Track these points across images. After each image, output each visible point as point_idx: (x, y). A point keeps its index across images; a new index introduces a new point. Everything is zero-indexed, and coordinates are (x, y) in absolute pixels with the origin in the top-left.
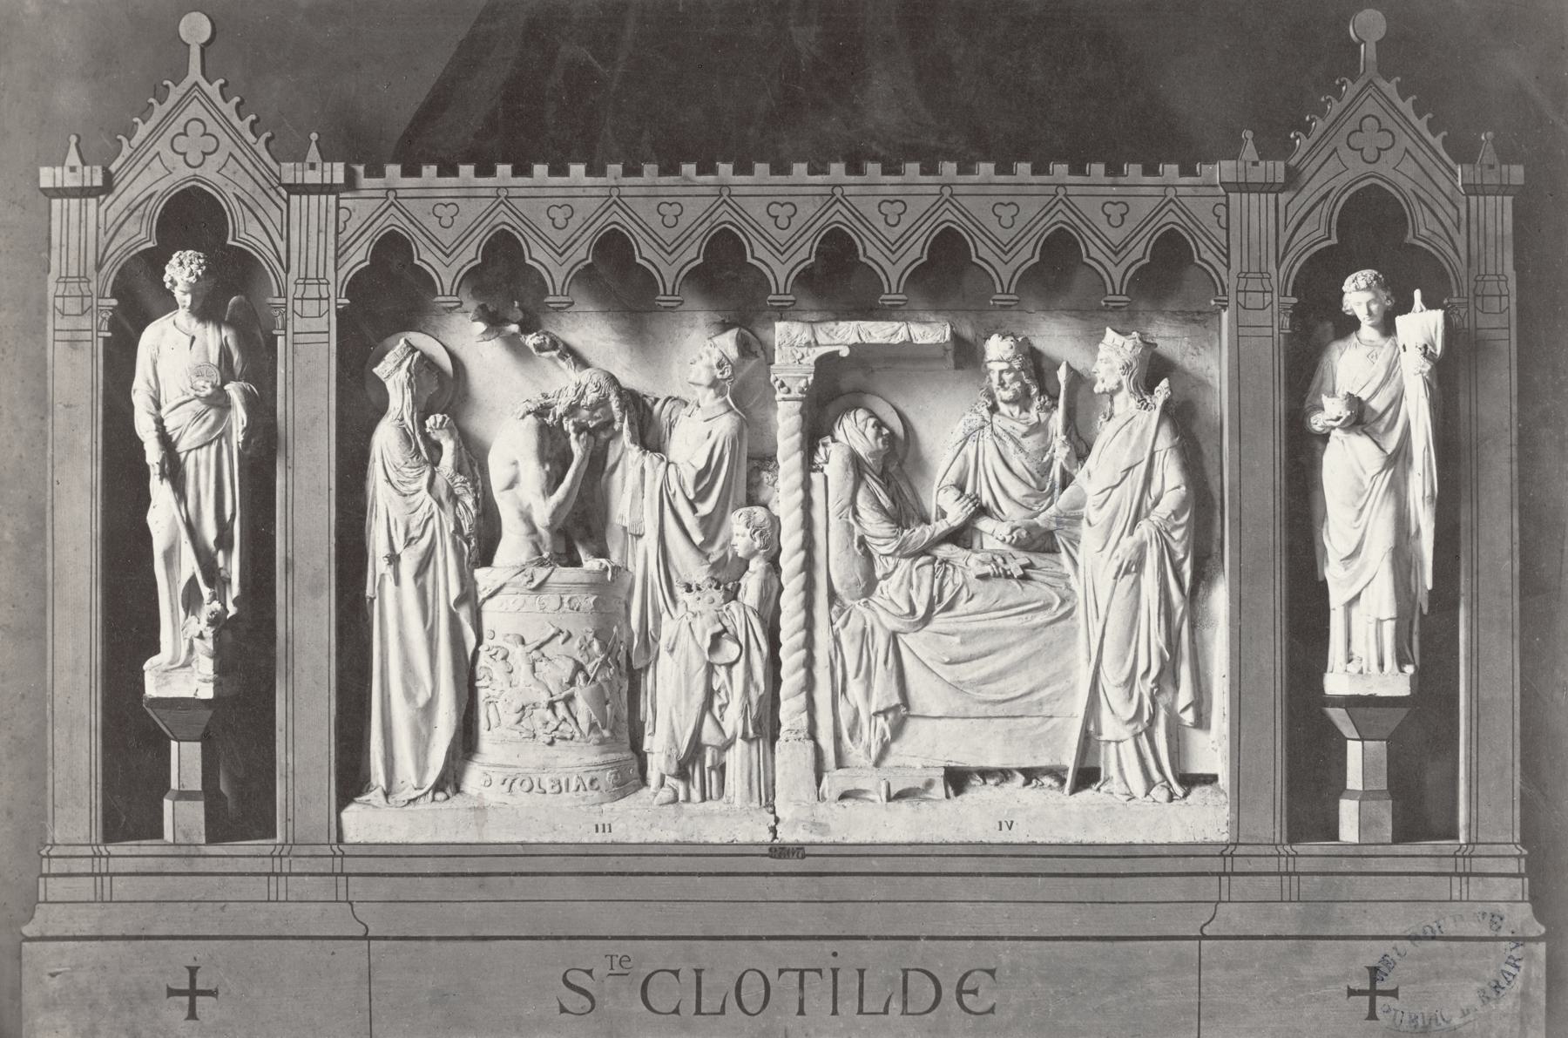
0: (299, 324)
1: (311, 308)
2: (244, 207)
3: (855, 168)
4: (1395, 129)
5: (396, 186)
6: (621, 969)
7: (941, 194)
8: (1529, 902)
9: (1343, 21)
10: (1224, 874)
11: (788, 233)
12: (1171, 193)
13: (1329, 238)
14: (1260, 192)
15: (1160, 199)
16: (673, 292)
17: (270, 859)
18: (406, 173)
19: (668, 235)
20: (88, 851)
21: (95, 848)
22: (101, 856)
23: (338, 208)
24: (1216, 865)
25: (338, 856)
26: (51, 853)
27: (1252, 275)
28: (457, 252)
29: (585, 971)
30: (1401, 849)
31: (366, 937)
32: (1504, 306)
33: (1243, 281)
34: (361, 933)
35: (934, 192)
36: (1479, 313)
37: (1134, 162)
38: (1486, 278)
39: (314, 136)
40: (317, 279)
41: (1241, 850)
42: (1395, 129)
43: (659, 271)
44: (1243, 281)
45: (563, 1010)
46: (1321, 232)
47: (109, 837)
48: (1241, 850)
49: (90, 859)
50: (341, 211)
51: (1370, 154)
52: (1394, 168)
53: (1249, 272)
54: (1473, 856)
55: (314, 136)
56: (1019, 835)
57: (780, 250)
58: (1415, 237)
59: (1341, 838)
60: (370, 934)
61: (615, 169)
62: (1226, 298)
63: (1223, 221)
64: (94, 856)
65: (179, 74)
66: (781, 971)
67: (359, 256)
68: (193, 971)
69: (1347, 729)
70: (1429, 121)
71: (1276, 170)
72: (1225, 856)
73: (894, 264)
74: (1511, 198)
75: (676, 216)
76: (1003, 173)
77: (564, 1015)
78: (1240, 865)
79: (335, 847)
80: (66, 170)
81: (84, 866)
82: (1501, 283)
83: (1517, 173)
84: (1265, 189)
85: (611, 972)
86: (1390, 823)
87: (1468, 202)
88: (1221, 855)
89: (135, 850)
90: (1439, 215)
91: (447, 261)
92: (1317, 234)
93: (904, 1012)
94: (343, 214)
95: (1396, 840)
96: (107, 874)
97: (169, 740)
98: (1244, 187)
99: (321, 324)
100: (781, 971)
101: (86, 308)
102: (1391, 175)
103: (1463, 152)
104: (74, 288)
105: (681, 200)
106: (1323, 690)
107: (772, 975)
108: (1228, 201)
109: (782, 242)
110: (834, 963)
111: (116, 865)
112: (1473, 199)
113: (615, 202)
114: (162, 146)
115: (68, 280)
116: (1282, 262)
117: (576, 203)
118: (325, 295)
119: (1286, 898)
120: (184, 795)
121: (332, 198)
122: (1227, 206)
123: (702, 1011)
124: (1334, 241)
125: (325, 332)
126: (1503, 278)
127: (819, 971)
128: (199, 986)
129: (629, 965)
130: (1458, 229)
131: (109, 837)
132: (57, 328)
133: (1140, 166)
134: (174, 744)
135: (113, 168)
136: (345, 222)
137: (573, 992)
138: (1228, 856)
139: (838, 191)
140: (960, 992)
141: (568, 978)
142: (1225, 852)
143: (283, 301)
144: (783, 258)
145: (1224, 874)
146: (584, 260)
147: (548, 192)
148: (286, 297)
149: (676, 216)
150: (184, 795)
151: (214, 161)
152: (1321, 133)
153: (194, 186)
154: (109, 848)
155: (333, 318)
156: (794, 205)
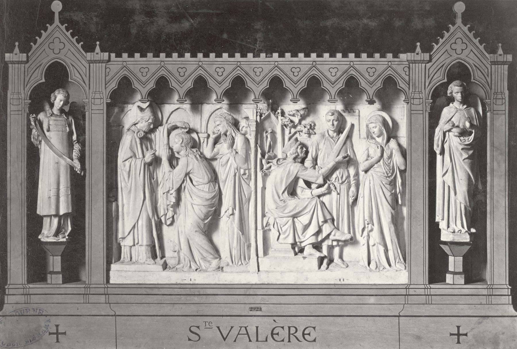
0: (94, 107)
4: (467, 43)
5: (126, 60)
7: (313, 64)
8: (512, 304)
11: (184, 78)
12: (125, 63)
14: (501, 65)
17: (84, 289)
19: (333, 79)
20: (423, 286)
21: (425, 285)
22: (428, 288)
23: (106, 69)
24: (403, 292)
26: (493, 288)
28: (147, 83)
29: (196, 327)
31: (115, 315)
33: (94, 94)
34: (114, 314)
36: (494, 105)
37: (88, 52)
38: (498, 93)
39: (17, 44)
41: (411, 286)
42: (467, 43)
43: (110, 91)
46: (39, 77)
48: (411, 286)
49: (104, 289)
51: (57, 51)
53: (415, 92)
54: (9, 289)
55: (17, 44)
56: (346, 282)
60: (116, 314)
63: (407, 74)
64: (425, 288)
65: (51, 22)
67: (113, 85)
68: (458, 327)
70: (76, 39)
71: (427, 56)
72: (488, 289)
73: (333, 88)
74: (507, 66)
76: (307, 57)
78: (412, 292)
80: (415, 54)
81: (422, 292)
82: (503, 95)
83: (510, 58)
84: (421, 62)
85: (206, 327)
98: (415, 62)
102: (63, 57)
103: (493, 51)
104: (15, 96)
105: (263, 66)
108: (409, 66)
109: (220, 81)
111: (433, 292)
112: (91, 65)
114: (448, 47)
118: (21, 98)
119: (26, 302)
122: (409, 68)
129: (212, 325)
130: (488, 76)
132: (412, 109)
133: (165, 54)
135: (29, 54)
136: (108, 72)
137: (193, 334)
138: (408, 288)
139: (352, 63)
142: (407, 287)
143: (88, 100)
144: (182, 86)
147: (330, 63)
151: (466, 52)
153: (56, 61)
154: (430, 285)
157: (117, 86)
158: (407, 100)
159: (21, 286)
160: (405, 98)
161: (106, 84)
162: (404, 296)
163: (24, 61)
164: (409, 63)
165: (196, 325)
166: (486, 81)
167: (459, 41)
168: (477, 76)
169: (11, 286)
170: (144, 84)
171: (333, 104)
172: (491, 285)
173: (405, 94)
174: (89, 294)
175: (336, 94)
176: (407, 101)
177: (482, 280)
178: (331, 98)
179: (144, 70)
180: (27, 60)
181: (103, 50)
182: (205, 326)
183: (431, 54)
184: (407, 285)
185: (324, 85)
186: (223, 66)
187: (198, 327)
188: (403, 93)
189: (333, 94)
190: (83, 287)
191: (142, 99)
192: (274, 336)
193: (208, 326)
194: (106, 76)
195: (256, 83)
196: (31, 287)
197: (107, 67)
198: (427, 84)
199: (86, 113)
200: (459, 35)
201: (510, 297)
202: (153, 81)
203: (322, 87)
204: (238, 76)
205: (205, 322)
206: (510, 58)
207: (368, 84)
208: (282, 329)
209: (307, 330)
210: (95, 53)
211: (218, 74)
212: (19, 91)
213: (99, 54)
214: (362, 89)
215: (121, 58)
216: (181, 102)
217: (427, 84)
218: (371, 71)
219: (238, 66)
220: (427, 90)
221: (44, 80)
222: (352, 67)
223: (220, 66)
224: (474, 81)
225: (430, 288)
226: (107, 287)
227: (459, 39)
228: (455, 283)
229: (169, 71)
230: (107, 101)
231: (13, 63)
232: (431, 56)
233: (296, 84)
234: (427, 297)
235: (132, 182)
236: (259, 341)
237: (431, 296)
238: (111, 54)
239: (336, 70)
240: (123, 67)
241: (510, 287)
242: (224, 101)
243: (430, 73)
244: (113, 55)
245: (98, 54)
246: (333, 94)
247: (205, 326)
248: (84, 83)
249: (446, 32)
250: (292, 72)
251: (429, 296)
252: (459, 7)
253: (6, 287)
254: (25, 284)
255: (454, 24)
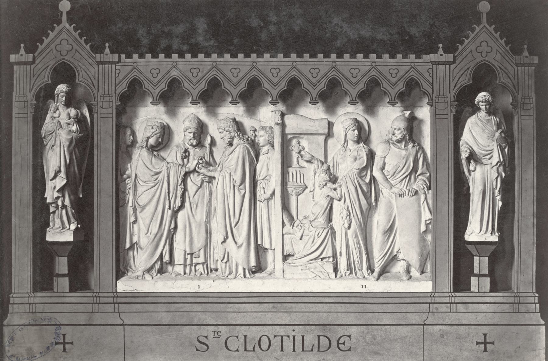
0: (103, 111)
1: (105, 105)
2: (502, 71)
3: (340, 56)
6: (217, 336)
7: (213, 65)
9: (475, 6)
10: (431, 303)
13: (470, 82)
15: (212, 66)
16: (156, 99)
17: (514, 298)
18: (193, 57)
19: (235, 80)
20: (27, 295)
25: (116, 297)
27: (20, 96)
30: (71, 294)
32: (111, 105)
35: (290, 64)
36: (436, 109)
40: (529, 97)
41: (436, 295)
44: (102, 98)
45: (197, 350)
47: (455, 290)
48: (436, 295)
50: (117, 71)
52: (72, 57)
57: (236, 85)
58: (79, 81)
59: (471, 291)
61: (399, 56)
62: (432, 102)
63: (431, 75)
65: (59, 22)
66: (275, 336)
67: (123, 88)
69: (474, 252)
70: (85, 40)
71: (450, 57)
72: (93, 297)
75: (317, 73)
76: (207, 57)
77: (198, 352)
78: (437, 300)
79: (115, 294)
80: (105, 55)
81: (26, 300)
83: (536, 60)
85: (214, 336)
86: (489, 284)
87: (98, 67)
88: (430, 297)
89: (82, 295)
90: (40, 72)
91: (194, 87)
92: (465, 81)
93: (319, 350)
94: (118, 71)
95: (491, 291)
96: (455, 303)
97: (473, 256)
98: (438, 63)
99: (110, 111)
100: (275, 336)
101: (111, 106)
102: (72, 60)
104: (441, 100)
105: (239, 67)
106: (464, 238)
107: (271, 337)
110: (293, 334)
111: (37, 300)
113: (294, 67)
115: (105, 96)
116: (32, 90)
117: (281, 68)
120: (480, 276)
121: (114, 66)
122: (432, 69)
123: (320, 350)
124: (471, 82)
125: (102, 114)
126: (25, 96)
127: (288, 336)
128: (488, 341)
130: (95, 79)
131: (455, 290)
134: (476, 259)
138: (94, 297)
140: (338, 344)
141: (199, 339)
142: (431, 295)
145: (431, 303)
146: (204, 88)
148: (97, 101)
149: (317, 73)
150: (480, 276)
152: (46, 45)
155: (114, 110)
156: (318, 69)
157: (405, 87)
158: (430, 103)
159: (27, 295)
160: (389, 100)
161: (115, 87)
162: (429, 304)
163: (536, 64)
164: (432, 65)
165: (204, 335)
166: (91, 82)
167: (64, 43)
168: (82, 78)
169: (15, 295)
170: (236, 85)
171: (235, 105)
172: (517, 293)
173: (429, 96)
174: (515, 303)
175: (238, 96)
176: (430, 104)
177: (507, 288)
178: (352, 99)
179: (195, 70)
180: (119, 60)
181: (112, 52)
182: (214, 335)
183: (456, 55)
184: (431, 294)
185: (363, 87)
186: (318, 67)
187: (206, 337)
188: (427, 96)
189: (314, 97)
190: (513, 296)
191: (233, 100)
192: (340, 345)
193: (216, 335)
194: (115, 77)
195: (273, 84)
196: (457, 296)
197: (116, 69)
198: (452, 88)
199: (95, 115)
200: (64, 36)
201: (538, 305)
202: (402, 83)
203: (382, 88)
204: (215, 77)
205: (213, 332)
206: (536, 60)
207: (391, 85)
208: (348, 338)
209: (342, 338)
210: (19, 55)
211: (391, 76)
212: (445, 95)
213: (24, 56)
214: (266, 91)
215: (250, 59)
216: (392, 104)
217: (452, 88)
218: (195, 71)
219: (215, 66)
220: (453, 93)
221: (50, 82)
222: (214, 68)
223: (236, 67)
224: (79, 82)
225: (117, 296)
226: (33, 296)
227: (64, 40)
228: (480, 291)
229: (260, 71)
230: (117, 104)
231: (19, 63)
232: (455, 57)
233: (155, 86)
234: (452, 305)
235: (159, 186)
236: (320, 351)
237: (117, 305)
238: (121, 55)
239: (197, 70)
240: (253, 68)
241: (537, 295)
242: (397, 103)
243: (35, 73)
244: (123, 56)
245: (107, 55)
246: (354, 96)
247: (214, 335)
248: (94, 86)
249: (51, 31)
250: (351, 73)
251: (115, 305)
252: (484, 7)
253: (11, 296)
254: (30, 293)
255: (478, 24)
